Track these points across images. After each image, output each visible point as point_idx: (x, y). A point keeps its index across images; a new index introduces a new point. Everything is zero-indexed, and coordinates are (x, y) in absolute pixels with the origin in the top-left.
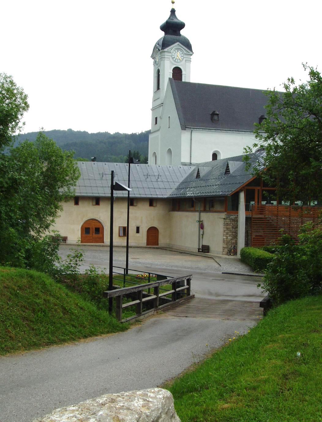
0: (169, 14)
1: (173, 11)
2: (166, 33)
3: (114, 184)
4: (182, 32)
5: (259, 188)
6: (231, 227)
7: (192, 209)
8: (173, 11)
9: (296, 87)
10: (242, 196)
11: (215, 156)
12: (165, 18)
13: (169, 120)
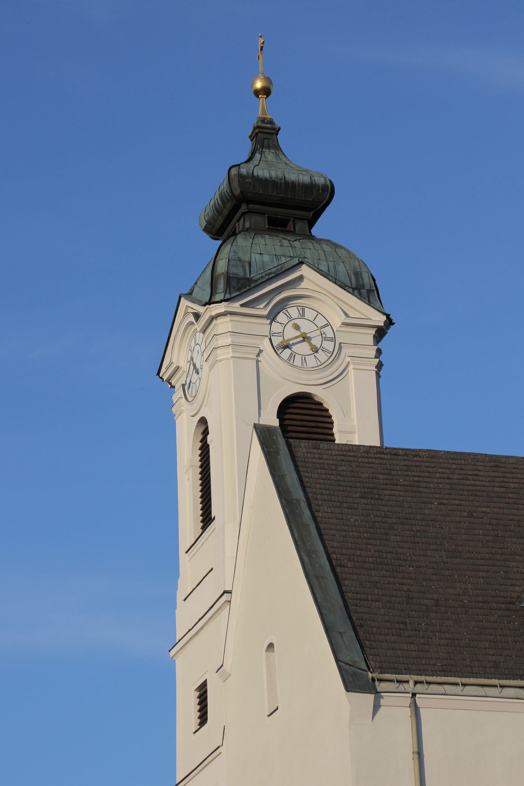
1: (265, 136)
8: (265, 136)
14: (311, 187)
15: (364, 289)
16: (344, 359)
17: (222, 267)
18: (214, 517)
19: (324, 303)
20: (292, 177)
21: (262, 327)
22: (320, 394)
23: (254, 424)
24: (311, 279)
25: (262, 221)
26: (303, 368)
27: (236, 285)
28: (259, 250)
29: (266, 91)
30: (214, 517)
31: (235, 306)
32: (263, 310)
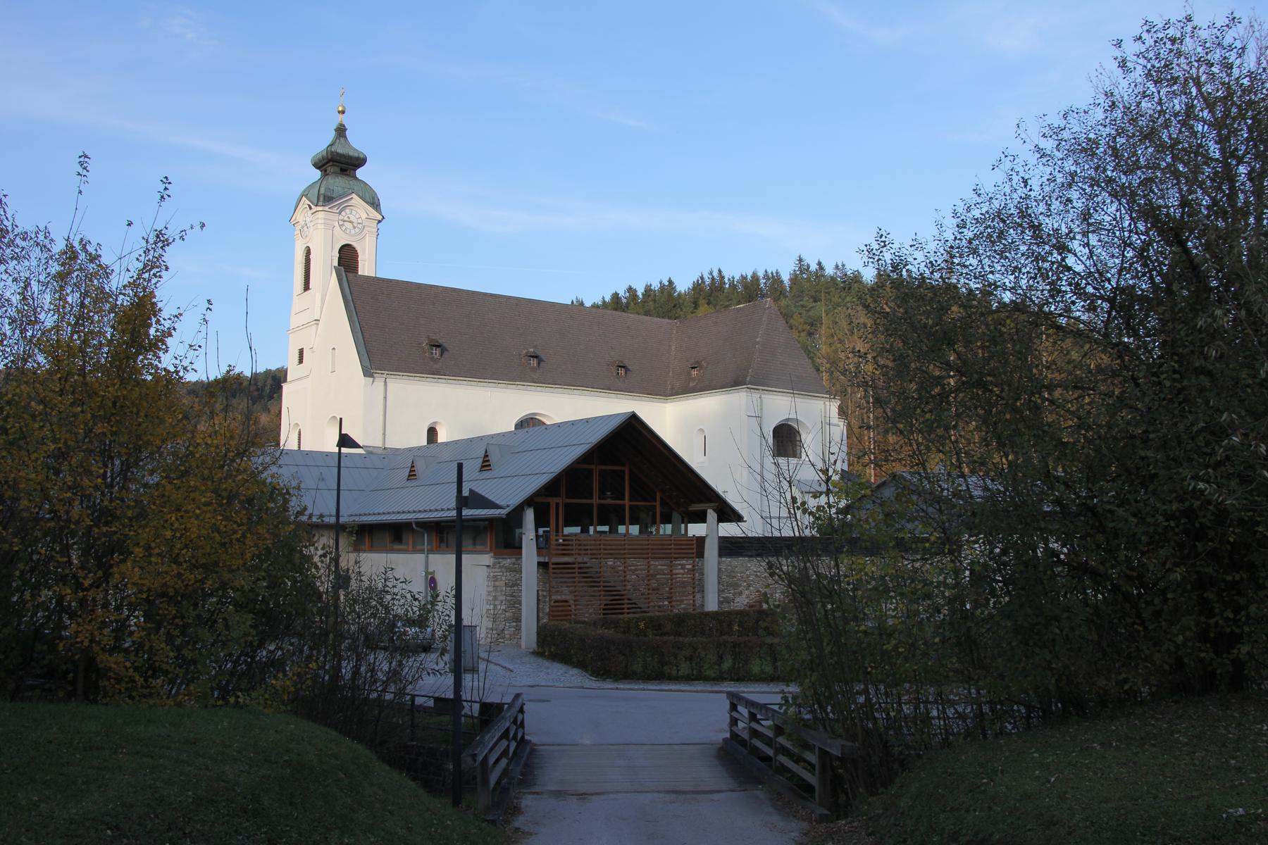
0: (331, 135)
1: (341, 131)
2: (325, 174)
3: (466, 493)
4: (360, 173)
5: (559, 500)
6: (502, 583)
7: (396, 547)
8: (341, 131)
9: (702, 278)
10: (529, 515)
11: (432, 432)
12: (322, 142)
13: (333, 356)
14: (358, 159)
15: (375, 204)
16: (365, 231)
17: (322, 191)
18: (819, 263)
19: (359, 209)
20: (351, 154)
21: (336, 217)
22: (354, 244)
23: (269, 386)
24: (356, 200)
25: (337, 169)
26: (350, 235)
27: (326, 199)
28: (337, 183)
29: (343, 112)
30: (819, 263)
31: (326, 208)
32: (334, 210)
